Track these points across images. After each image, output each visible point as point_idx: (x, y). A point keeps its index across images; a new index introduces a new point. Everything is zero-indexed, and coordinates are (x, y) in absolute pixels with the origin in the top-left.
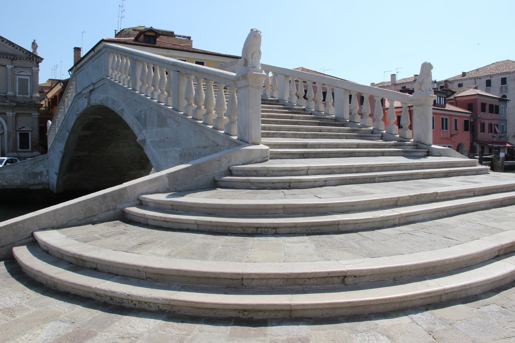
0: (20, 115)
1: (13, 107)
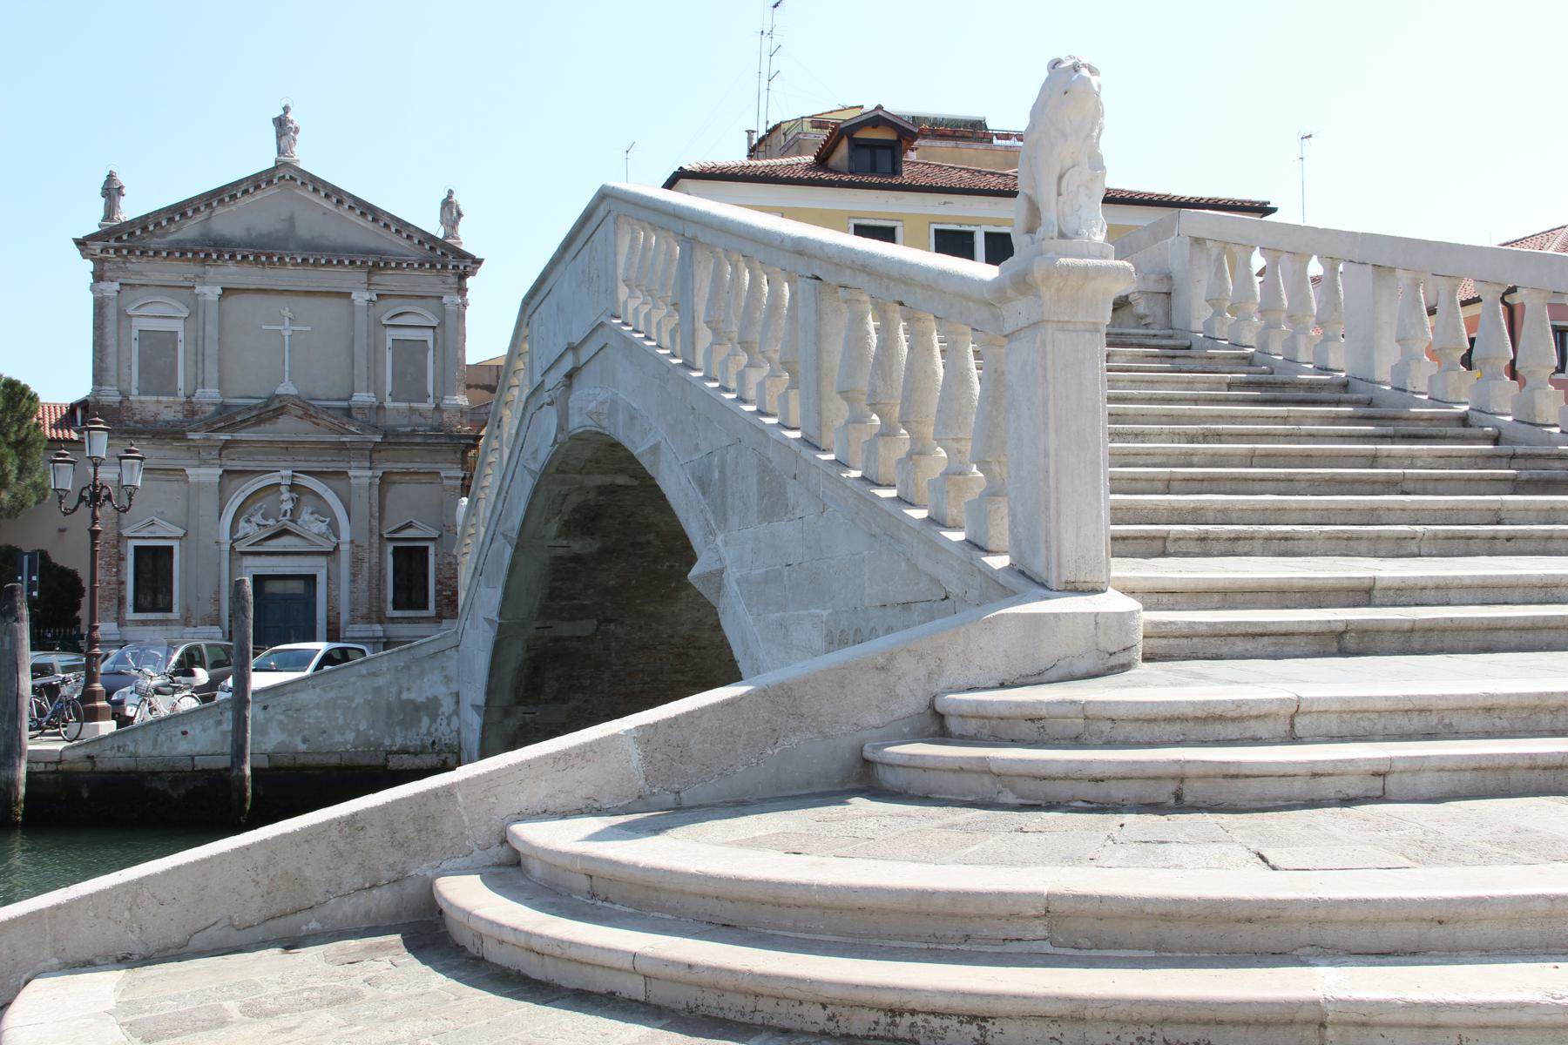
0: (396, 478)
1: (372, 451)
